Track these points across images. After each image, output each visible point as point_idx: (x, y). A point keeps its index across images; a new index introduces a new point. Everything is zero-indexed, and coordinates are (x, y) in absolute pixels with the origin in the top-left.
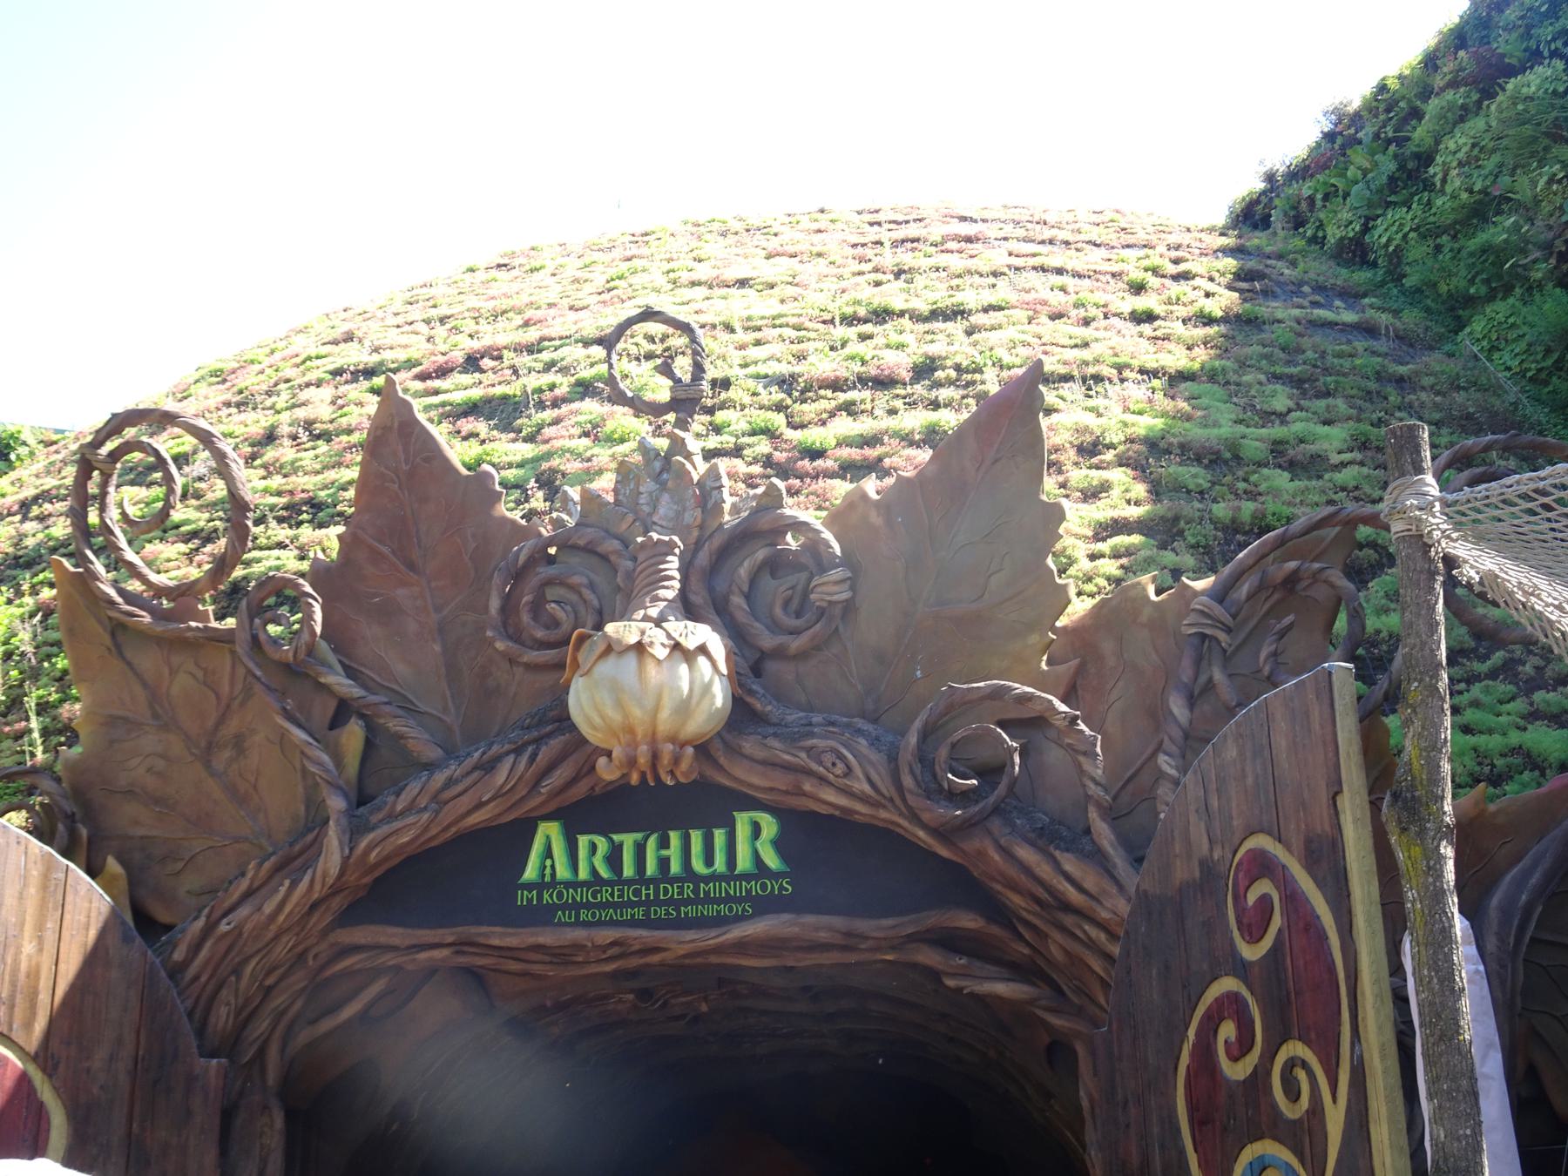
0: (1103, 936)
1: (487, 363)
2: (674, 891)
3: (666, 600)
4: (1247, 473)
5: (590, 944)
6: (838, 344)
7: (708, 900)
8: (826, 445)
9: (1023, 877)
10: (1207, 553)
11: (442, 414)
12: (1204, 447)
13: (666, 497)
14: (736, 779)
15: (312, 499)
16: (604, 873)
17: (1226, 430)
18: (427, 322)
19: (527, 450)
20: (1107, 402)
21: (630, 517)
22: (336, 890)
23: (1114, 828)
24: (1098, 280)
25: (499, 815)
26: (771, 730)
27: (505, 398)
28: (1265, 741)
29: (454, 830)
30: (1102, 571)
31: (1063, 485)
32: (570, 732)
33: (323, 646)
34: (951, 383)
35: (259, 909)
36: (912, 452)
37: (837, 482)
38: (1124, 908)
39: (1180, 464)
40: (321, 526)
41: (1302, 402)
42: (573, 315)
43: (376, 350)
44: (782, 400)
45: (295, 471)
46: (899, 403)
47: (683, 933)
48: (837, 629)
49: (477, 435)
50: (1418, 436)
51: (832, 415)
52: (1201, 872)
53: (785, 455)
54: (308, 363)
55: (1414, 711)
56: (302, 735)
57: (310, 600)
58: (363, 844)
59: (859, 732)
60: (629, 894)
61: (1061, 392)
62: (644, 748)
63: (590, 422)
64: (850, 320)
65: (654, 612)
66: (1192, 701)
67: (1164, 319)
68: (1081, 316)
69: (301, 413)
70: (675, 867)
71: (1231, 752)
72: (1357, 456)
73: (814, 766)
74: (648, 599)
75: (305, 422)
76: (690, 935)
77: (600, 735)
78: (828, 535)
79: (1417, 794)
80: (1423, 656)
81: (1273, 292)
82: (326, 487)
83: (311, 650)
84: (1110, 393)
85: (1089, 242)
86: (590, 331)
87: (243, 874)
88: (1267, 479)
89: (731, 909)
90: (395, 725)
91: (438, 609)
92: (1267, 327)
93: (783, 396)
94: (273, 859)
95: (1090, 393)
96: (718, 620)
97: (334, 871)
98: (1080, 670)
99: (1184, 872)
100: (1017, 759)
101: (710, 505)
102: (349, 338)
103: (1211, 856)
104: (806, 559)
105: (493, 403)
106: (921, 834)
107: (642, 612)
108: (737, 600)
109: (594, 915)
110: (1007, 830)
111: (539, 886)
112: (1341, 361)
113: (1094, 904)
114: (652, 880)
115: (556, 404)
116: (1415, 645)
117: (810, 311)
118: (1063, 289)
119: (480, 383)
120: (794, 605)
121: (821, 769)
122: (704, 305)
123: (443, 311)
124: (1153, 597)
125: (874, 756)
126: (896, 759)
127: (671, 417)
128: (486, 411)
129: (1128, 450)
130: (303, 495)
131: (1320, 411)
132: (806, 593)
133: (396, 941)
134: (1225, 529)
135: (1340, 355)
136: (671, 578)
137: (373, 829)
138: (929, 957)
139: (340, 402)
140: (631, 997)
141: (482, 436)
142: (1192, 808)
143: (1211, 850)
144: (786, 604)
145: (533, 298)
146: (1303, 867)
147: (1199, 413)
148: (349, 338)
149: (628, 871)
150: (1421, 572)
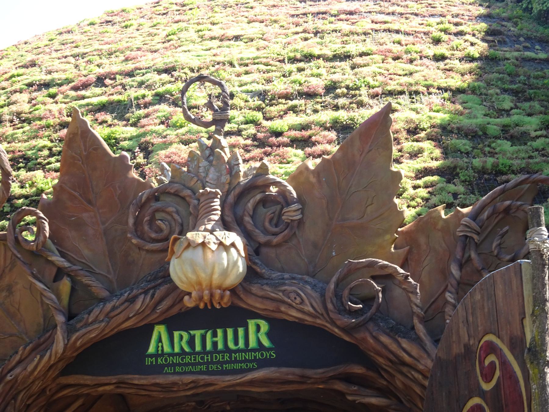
0: (420, 377)
1: (108, 81)
2: (220, 357)
3: (214, 221)
4: (490, 142)
5: (181, 383)
6: (287, 74)
7: (236, 361)
8: (283, 130)
9: (384, 350)
10: (470, 185)
11: (88, 110)
12: (469, 130)
13: (212, 169)
14: (248, 305)
15: (24, 155)
16: (187, 349)
17: (480, 120)
18: (74, 56)
19: (132, 131)
20: (421, 106)
21: (195, 179)
22: (60, 360)
23: (425, 327)
24: (417, 37)
25: (138, 323)
26: (265, 281)
27: (119, 102)
28: (493, 293)
29: (116, 330)
30: (419, 195)
31: (400, 151)
32: (170, 283)
33: (49, 242)
34: (344, 95)
35: (25, 369)
36: (326, 133)
37: (289, 149)
38: (430, 364)
39: (457, 139)
40: (30, 170)
41: (518, 104)
42: (150, 56)
43: (50, 72)
44: (260, 105)
45: (13, 140)
46: (318, 107)
47: (223, 377)
48: (295, 233)
49: (106, 122)
50: (539, 212)
51: (286, 113)
52: (465, 349)
53: (263, 134)
54: (13, 79)
55: (536, 318)
56: (42, 286)
57: (43, 221)
58: (74, 338)
59: (306, 282)
60: (199, 359)
61: (399, 100)
62: (206, 292)
63: (164, 116)
64: (293, 60)
65: (209, 227)
66: (461, 266)
67: (450, 59)
68: (408, 58)
69: (14, 108)
70: (220, 346)
71: (478, 297)
72: (544, 132)
73: (286, 299)
74: (206, 220)
75: (17, 113)
76: (228, 378)
77: (185, 286)
78: (290, 188)
79: (537, 349)
80: (540, 297)
81: (504, 41)
82: (30, 149)
83: (44, 243)
84: (423, 100)
85: (412, 14)
86: (160, 65)
87: (17, 353)
88: (500, 145)
89: (247, 366)
90: (86, 281)
91: (103, 223)
92: (501, 63)
93: (260, 102)
94: (31, 345)
95: (413, 100)
96: (238, 228)
97: (60, 351)
98: (409, 252)
99: (457, 349)
100: (380, 295)
101: (233, 173)
102: (33, 64)
103: (469, 343)
104: (280, 199)
105: (113, 105)
106: (336, 330)
107: (203, 227)
108: (247, 219)
109: (182, 369)
110: (376, 329)
111: (156, 356)
112: (538, 81)
113: (416, 362)
114: (210, 352)
115: (146, 106)
116: (537, 292)
117: (272, 55)
118: (399, 43)
119: (106, 93)
120: (275, 221)
121: (289, 300)
122: (218, 51)
123: (81, 50)
124: (444, 217)
125: (314, 294)
126: (324, 296)
127: (213, 128)
128: (110, 109)
129: (432, 131)
130: (19, 153)
131: (527, 109)
132: (280, 215)
133: (89, 382)
134: (479, 172)
135: (536, 78)
136: (217, 210)
137: (78, 331)
138: (340, 386)
139: (33, 102)
140: (193, 404)
141: (109, 122)
142: (461, 321)
143: (469, 340)
144: (271, 220)
145: (128, 44)
146: (509, 350)
147: (467, 111)
148: (33, 64)
149: (198, 348)
150: (540, 264)
